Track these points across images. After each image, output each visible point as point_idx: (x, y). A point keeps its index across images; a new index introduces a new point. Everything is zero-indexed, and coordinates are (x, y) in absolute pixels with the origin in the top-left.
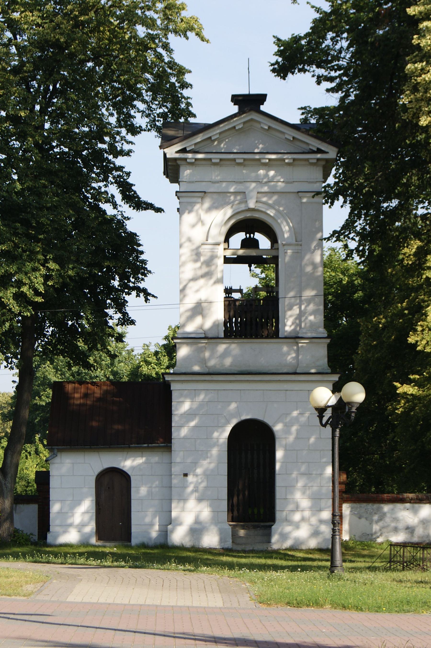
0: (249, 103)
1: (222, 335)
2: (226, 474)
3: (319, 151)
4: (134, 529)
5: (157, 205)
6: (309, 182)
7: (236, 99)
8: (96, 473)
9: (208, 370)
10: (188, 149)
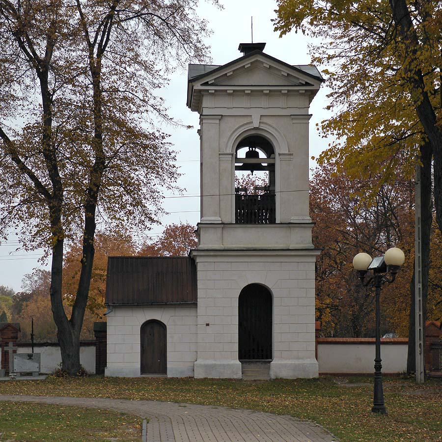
0: (252, 50)
3: (307, 84)
4: (169, 366)
7: (243, 47)
8: (141, 324)
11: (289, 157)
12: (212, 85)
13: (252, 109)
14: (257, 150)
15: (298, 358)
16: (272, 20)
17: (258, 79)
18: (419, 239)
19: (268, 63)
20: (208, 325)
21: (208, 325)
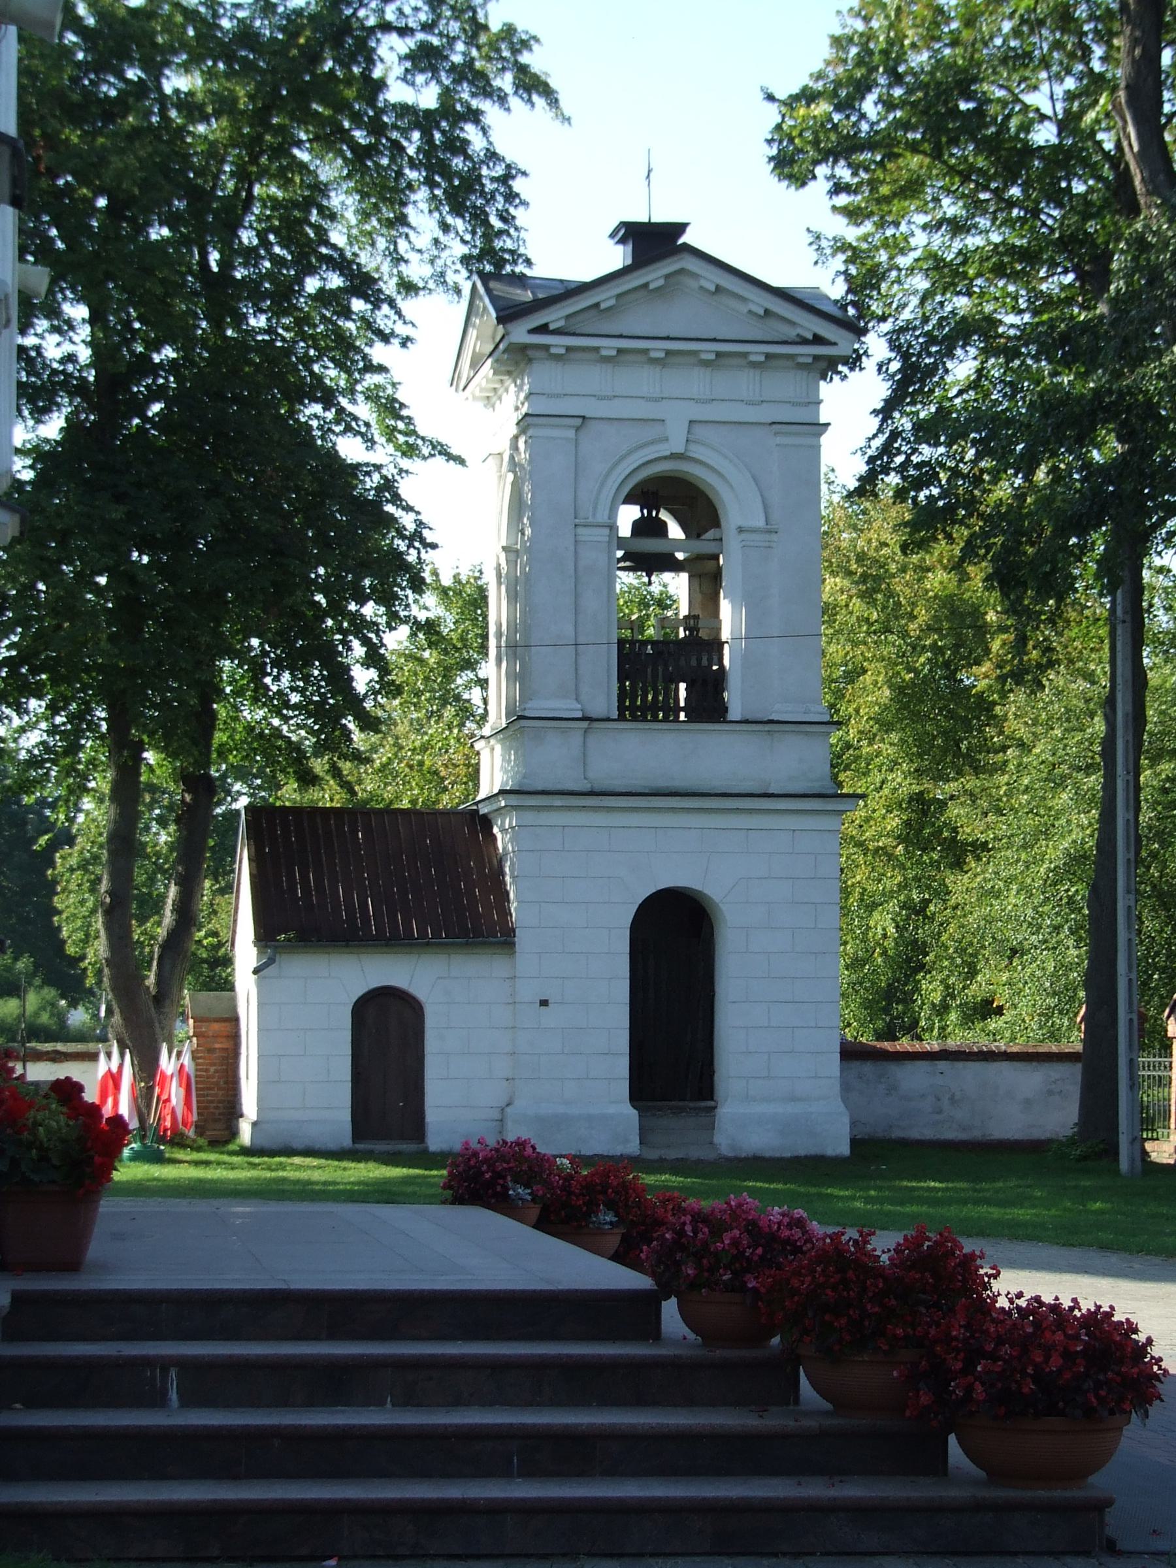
1: (615, 714)
2: (348, 1077)
3: (818, 340)
4: (432, 1116)
5: (454, 451)
6: (794, 404)
9: (589, 786)
10: (552, 327)
11: (767, 537)
12: (558, 332)
13: (616, 400)
14: (664, 515)
15: (794, 1099)
16: (816, 263)
17: (682, 316)
18: (1128, 773)
19: (806, 324)
20: (544, 1003)
21: (544, 1003)
